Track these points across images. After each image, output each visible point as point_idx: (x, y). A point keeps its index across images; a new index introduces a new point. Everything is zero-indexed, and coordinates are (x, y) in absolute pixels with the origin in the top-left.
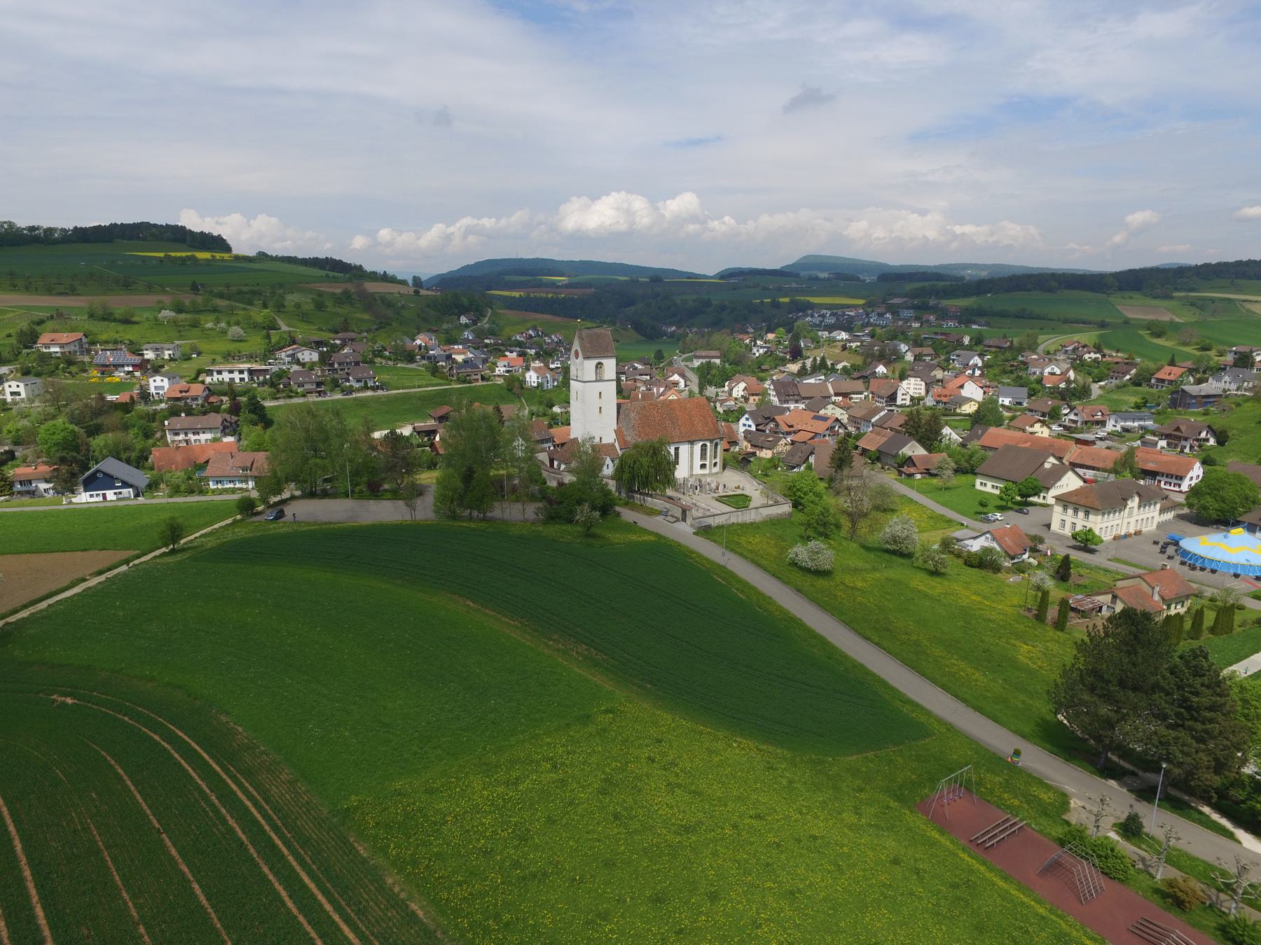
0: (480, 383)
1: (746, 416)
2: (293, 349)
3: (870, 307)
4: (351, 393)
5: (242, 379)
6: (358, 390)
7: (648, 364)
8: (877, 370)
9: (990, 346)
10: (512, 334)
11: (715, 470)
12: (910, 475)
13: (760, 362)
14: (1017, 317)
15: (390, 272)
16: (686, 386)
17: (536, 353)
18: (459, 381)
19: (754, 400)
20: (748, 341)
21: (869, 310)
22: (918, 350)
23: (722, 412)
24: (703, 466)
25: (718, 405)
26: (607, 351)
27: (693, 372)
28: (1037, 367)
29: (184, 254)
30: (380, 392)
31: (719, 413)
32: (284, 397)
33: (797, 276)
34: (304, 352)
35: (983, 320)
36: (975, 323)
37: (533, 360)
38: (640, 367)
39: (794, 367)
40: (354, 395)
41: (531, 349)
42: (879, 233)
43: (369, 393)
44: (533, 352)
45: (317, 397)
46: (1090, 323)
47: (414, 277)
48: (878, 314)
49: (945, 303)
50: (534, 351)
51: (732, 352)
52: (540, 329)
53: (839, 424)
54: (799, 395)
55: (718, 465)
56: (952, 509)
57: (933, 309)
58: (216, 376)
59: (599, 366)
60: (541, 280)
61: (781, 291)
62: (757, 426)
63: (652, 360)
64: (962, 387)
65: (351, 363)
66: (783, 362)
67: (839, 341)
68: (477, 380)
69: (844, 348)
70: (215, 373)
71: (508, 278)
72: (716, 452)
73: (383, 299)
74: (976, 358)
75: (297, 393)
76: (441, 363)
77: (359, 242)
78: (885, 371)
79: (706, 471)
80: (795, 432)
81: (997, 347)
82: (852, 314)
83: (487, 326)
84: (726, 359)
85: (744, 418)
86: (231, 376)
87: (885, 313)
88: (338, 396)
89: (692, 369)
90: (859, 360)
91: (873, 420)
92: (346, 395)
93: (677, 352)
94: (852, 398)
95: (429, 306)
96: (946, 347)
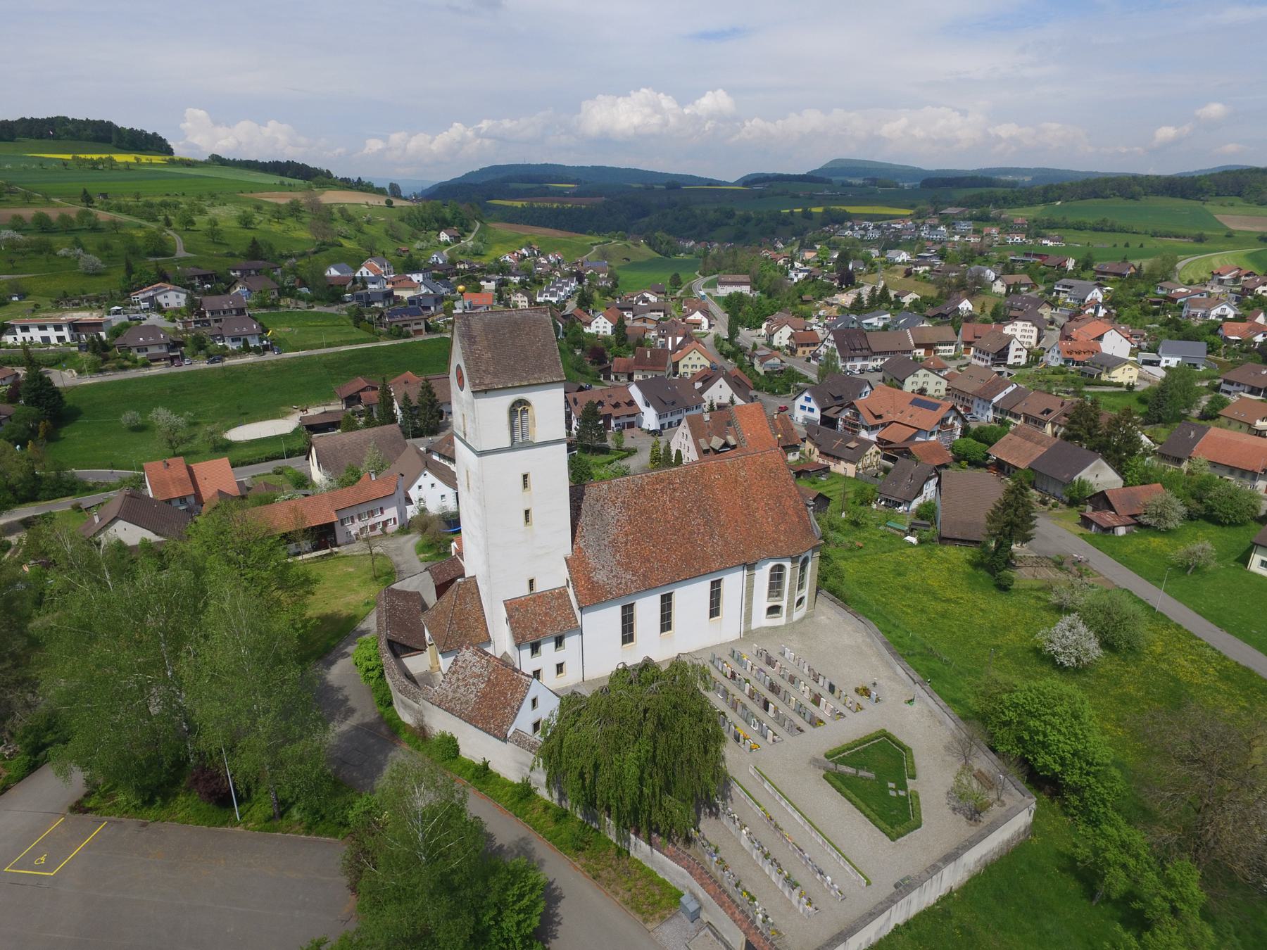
0: (426, 337)
1: (807, 394)
2: (155, 290)
3: (919, 218)
4: (221, 360)
5: (61, 339)
6: (234, 354)
7: (662, 293)
8: (960, 307)
9: (1105, 273)
10: (501, 253)
11: (798, 614)
12: (1110, 530)
13: (799, 290)
14: (1095, 230)
15: (365, 179)
16: (710, 326)
17: (521, 282)
18: (392, 335)
19: (804, 352)
20: (781, 262)
21: (919, 221)
22: (1012, 279)
23: (762, 373)
24: (774, 610)
25: (756, 362)
26: (542, 370)
27: (719, 304)
28: (1199, 307)
29: (95, 157)
30: (270, 356)
31: (758, 374)
32: (114, 369)
33: (829, 182)
34: (168, 294)
35: (1055, 233)
36: (1044, 237)
37: (517, 291)
38: (653, 299)
39: (846, 299)
40: (228, 362)
41: (515, 276)
42: (918, 132)
43: (251, 358)
44: (516, 280)
45: (167, 366)
46: (1184, 237)
47: (391, 184)
48: (930, 226)
49: (1007, 214)
50: (518, 278)
51: (765, 276)
52: (536, 247)
53: (954, 414)
54: (869, 349)
55: (806, 601)
56: (1247, 639)
57: (995, 221)
58: (20, 335)
59: (519, 409)
60: (547, 188)
61: (813, 199)
62: (822, 410)
63: (667, 288)
64: (1100, 338)
65: (230, 311)
66: (830, 291)
67: (899, 264)
68: (418, 332)
69: (908, 273)
70: (18, 330)
71: (513, 185)
72: (802, 578)
73: (343, 211)
74: (1096, 290)
75: (135, 361)
76: (376, 305)
77: (374, 145)
78: (971, 308)
79: (780, 620)
80: (884, 425)
81: (1116, 274)
82: (899, 226)
83: (470, 244)
84: (757, 286)
85: (802, 398)
86: (44, 333)
87: (939, 226)
88: (202, 365)
89: (717, 299)
90: (932, 292)
91: (995, 400)
92: (212, 362)
93: (697, 273)
94: (938, 351)
95: (402, 220)
96: (1045, 274)
